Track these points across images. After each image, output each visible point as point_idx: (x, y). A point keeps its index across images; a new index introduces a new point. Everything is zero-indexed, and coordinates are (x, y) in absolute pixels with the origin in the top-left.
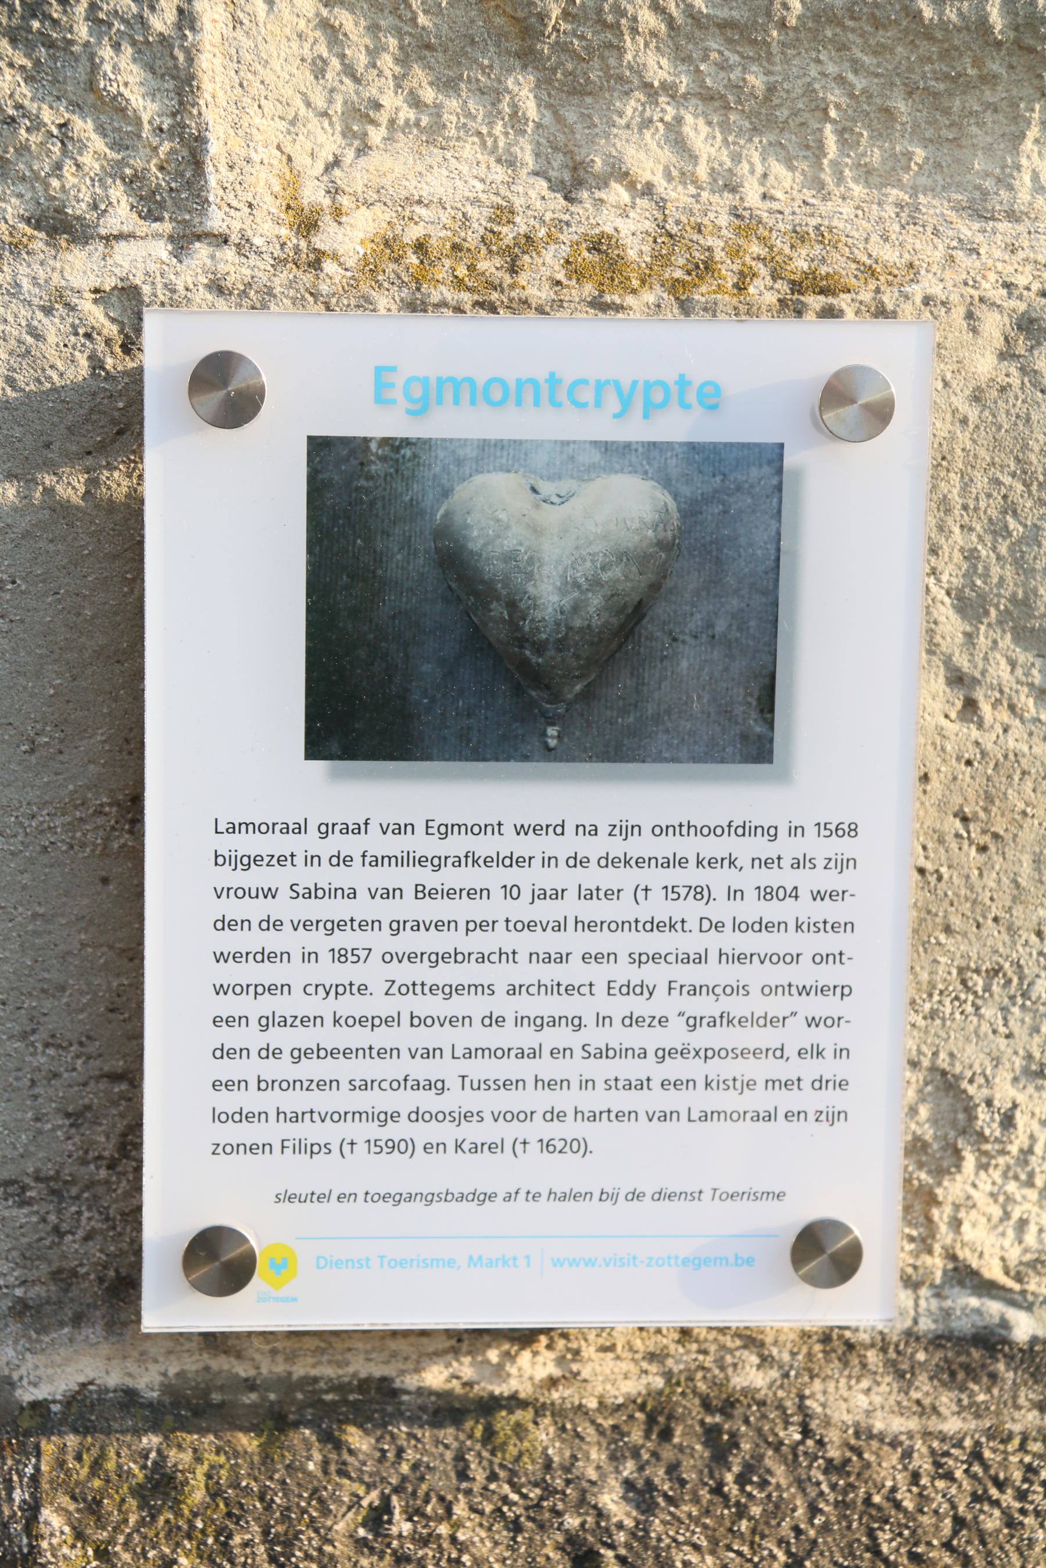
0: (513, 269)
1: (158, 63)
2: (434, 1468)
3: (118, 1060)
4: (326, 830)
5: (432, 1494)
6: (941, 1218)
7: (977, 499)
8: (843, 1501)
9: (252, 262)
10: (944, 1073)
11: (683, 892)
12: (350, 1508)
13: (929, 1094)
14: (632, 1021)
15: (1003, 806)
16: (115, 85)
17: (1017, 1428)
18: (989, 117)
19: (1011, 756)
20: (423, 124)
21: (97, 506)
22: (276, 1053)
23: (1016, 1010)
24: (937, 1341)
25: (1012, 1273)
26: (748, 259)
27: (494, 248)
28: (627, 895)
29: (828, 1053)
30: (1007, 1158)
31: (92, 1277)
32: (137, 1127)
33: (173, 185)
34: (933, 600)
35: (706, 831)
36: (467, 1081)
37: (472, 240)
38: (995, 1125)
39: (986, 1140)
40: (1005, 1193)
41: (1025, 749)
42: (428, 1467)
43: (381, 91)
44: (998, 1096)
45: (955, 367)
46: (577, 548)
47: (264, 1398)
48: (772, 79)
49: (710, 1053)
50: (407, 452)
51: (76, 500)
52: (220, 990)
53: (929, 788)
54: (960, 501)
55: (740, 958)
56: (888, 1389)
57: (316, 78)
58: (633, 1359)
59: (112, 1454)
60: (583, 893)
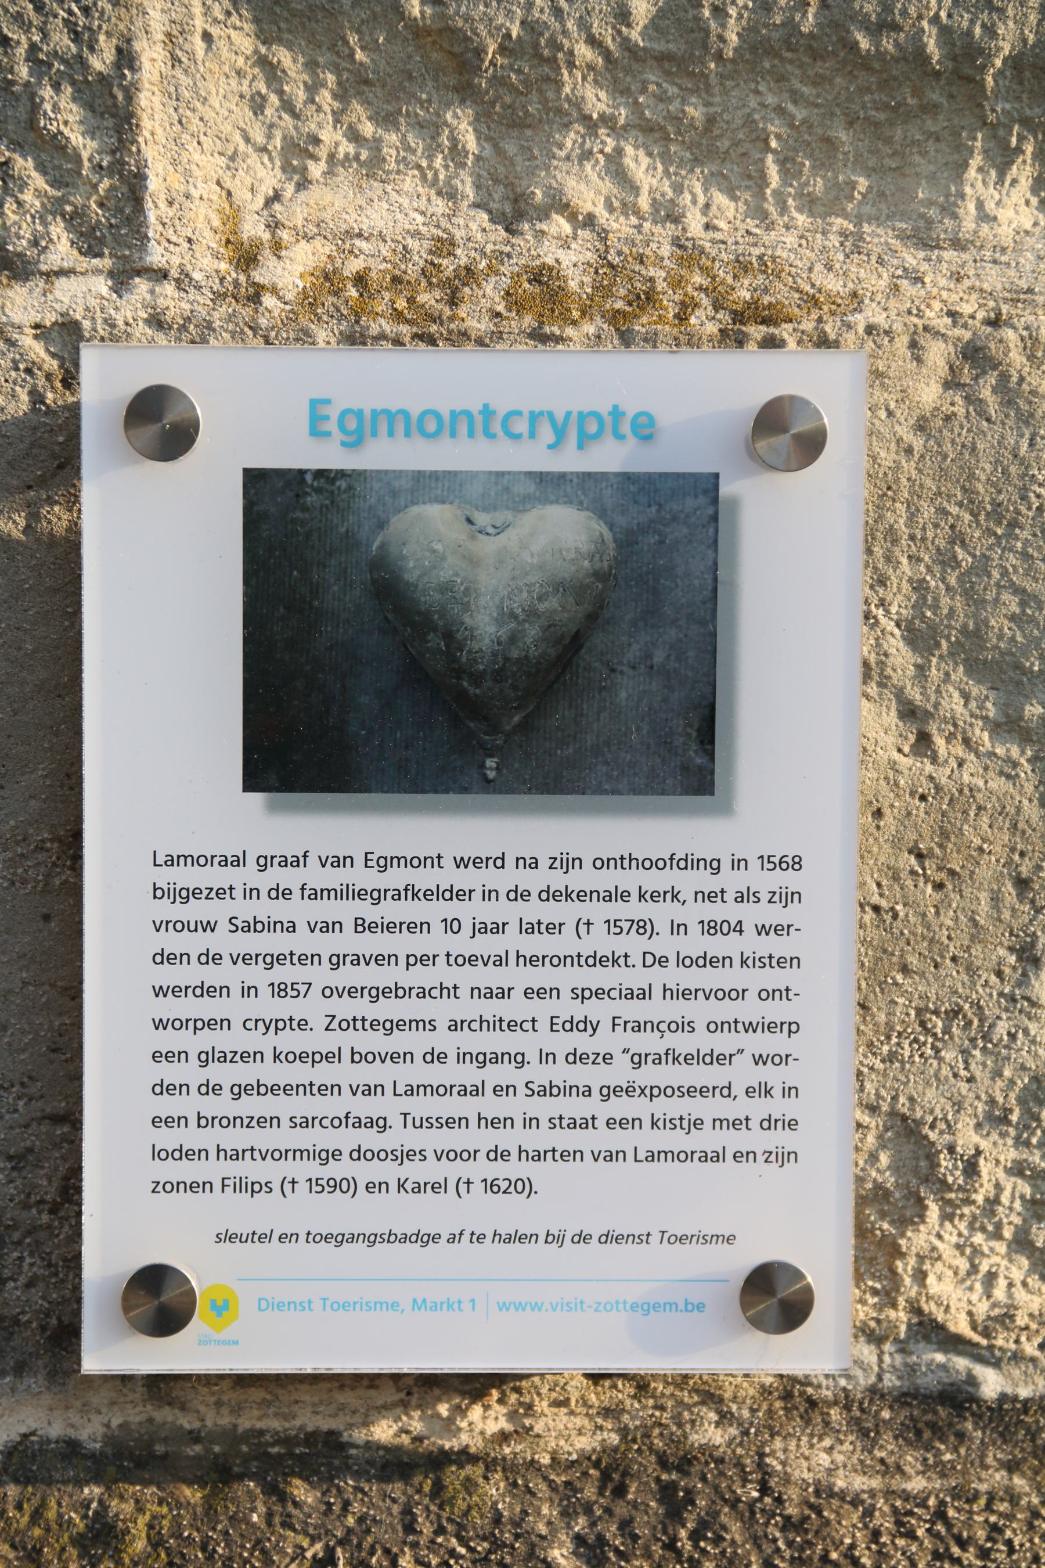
0: (453, 301)
1: (98, 101)
2: (381, 1521)
3: (60, 1101)
4: (264, 863)
5: (377, 1546)
6: (905, 1270)
7: (924, 529)
8: (800, 1558)
9: (191, 297)
10: (904, 1118)
11: (626, 926)
12: (293, 1560)
13: (889, 1139)
14: (576, 1057)
15: (959, 842)
16: (55, 123)
17: (983, 1487)
18: (931, 146)
19: (966, 791)
20: (363, 158)
21: (38, 540)
22: (216, 1089)
23: (977, 1053)
24: (903, 1399)
25: (979, 1329)
26: (690, 289)
27: (434, 280)
28: (569, 929)
29: (777, 1092)
30: (973, 1208)
31: (34, 1325)
32: (76, 1171)
33: (113, 221)
34: (882, 631)
35: (647, 864)
36: (409, 1118)
37: (412, 272)
38: (958, 1173)
39: (949, 1188)
40: (972, 1245)
41: (981, 783)
42: (374, 1520)
43: (320, 126)
44: (960, 1142)
45: (899, 396)
46: (513, 578)
47: (208, 1451)
48: (712, 110)
49: (656, 1092)
50: (343, 484)
51: (17, 534)
52: (160, 1024)
53: (882, 823)
54: (907, 531)
55: (685, 994)
56: (851, 1448)
57: (255, 114)
58: (587, 1414)
59: (53, 1503)
60: (524, 927)
